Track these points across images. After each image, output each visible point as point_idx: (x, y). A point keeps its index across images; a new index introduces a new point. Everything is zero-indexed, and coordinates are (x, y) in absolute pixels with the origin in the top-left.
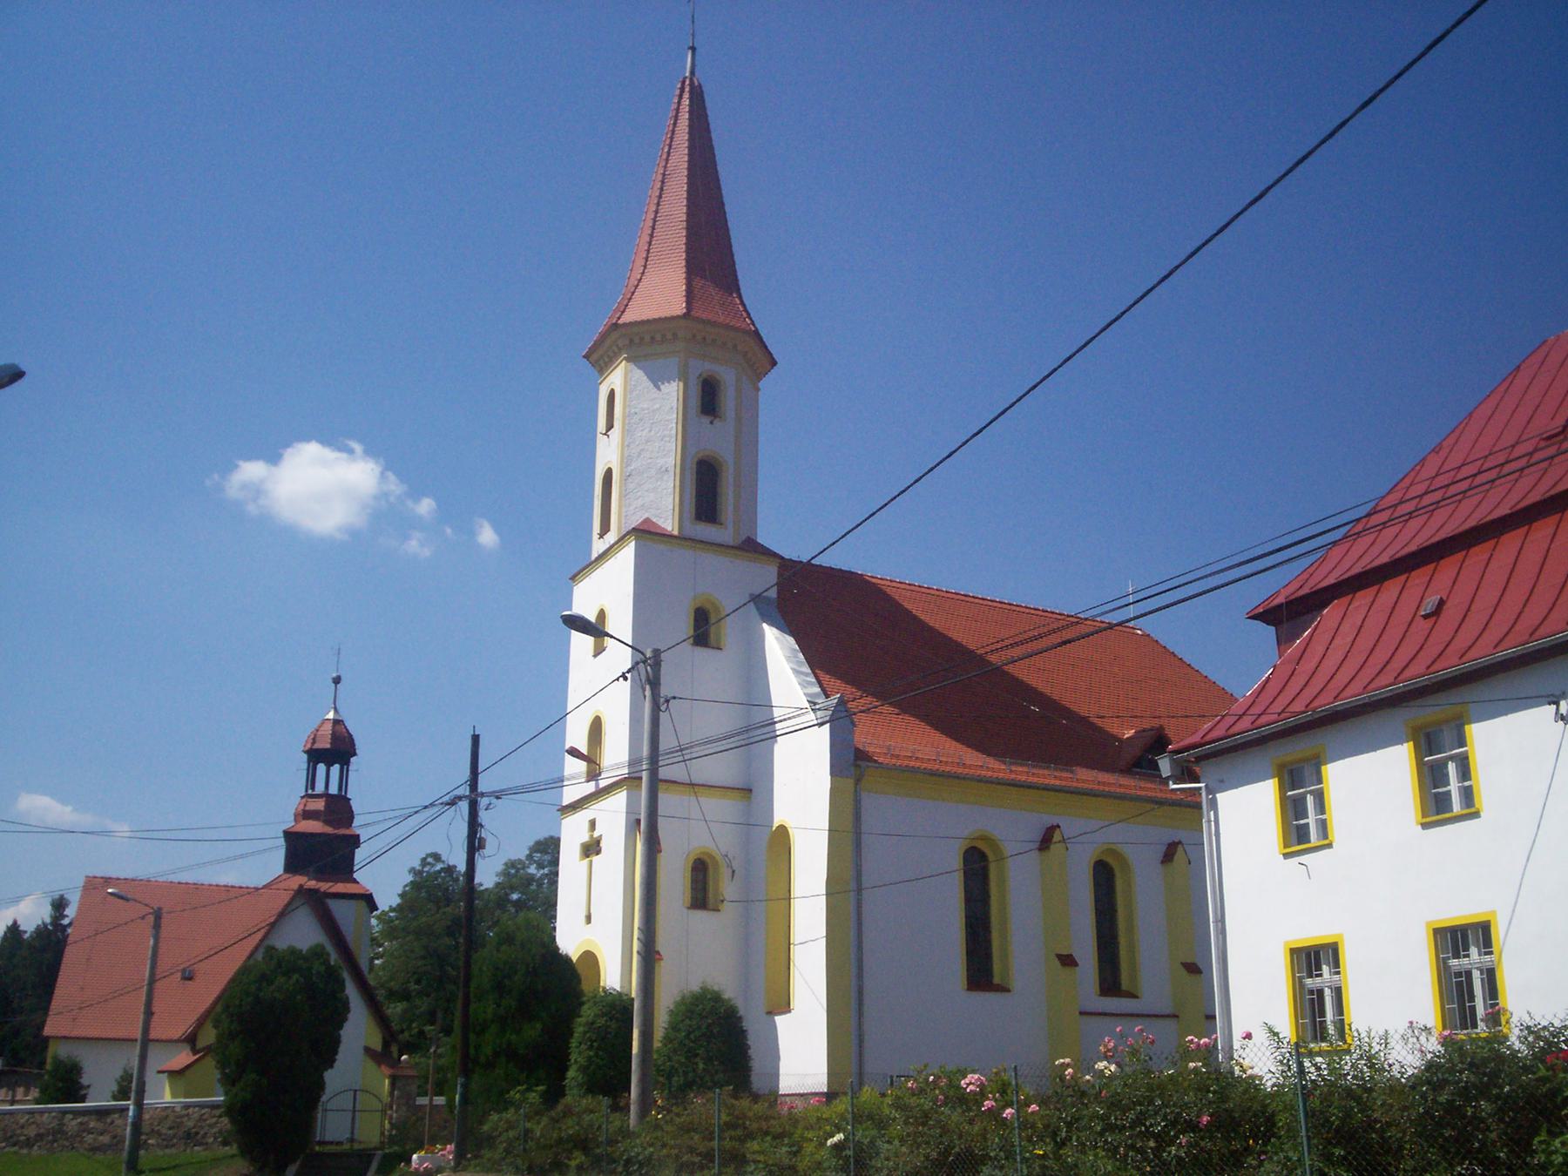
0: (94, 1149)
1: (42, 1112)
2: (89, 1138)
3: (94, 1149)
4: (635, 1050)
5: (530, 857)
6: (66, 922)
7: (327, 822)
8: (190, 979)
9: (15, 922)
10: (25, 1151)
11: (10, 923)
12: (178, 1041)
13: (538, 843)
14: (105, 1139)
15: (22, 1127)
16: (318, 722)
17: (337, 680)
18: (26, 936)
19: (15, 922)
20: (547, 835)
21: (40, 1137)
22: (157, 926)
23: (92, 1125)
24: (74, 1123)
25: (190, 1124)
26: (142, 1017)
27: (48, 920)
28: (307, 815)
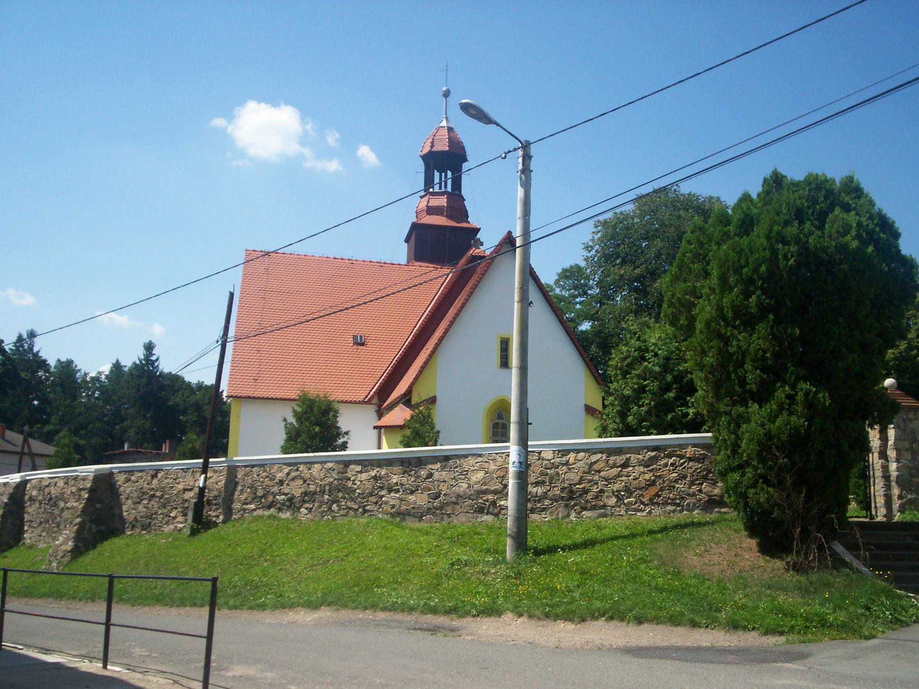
0: (401, 515)
1: (310, 464)
2: (391, 499)
3: (401, 515)
4: (317, 454)
5: (557, 282)
6: (154, 358)
7: (449, 217)
8: (363, 344)
9: (118, 361)
10: (286, 515)
11: (114, 361)
12: (363, 402)
13: (565, 271)
14: (420, 499)
15: (281, 482)
16: (434, 130)
17: (447, 94)
18: (126, 369)
19: (118, 361)
20: (806, 174)
21: (308, 496)
22: (527, 158)
23: (395, 479)
24: (364, 476)
25: (574, 477)
26: (516, 307)
27: (142, 357)
28: (431, 211)
